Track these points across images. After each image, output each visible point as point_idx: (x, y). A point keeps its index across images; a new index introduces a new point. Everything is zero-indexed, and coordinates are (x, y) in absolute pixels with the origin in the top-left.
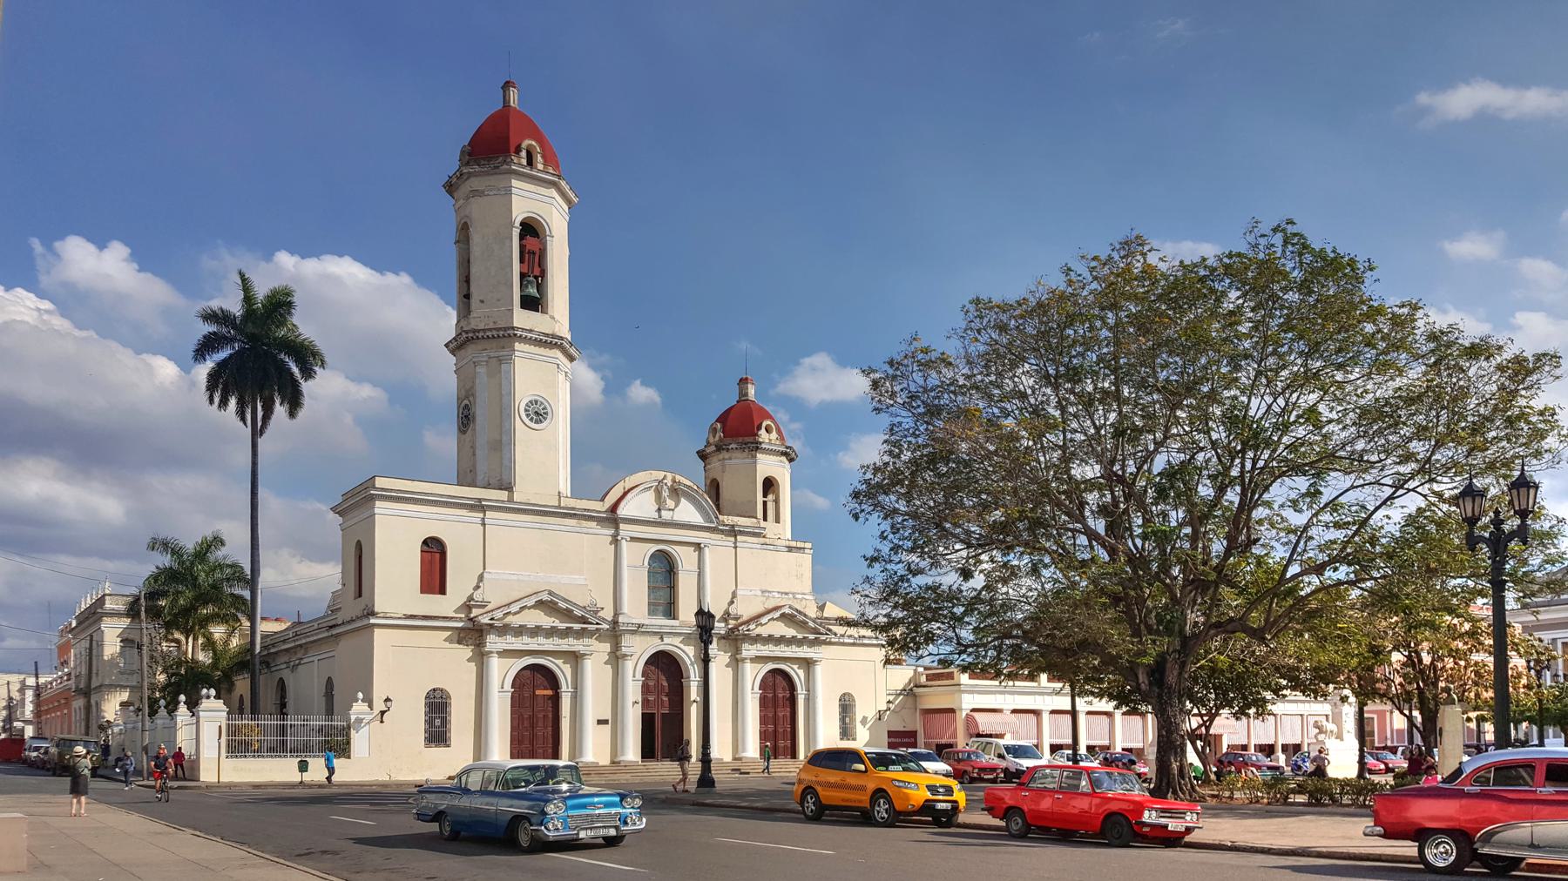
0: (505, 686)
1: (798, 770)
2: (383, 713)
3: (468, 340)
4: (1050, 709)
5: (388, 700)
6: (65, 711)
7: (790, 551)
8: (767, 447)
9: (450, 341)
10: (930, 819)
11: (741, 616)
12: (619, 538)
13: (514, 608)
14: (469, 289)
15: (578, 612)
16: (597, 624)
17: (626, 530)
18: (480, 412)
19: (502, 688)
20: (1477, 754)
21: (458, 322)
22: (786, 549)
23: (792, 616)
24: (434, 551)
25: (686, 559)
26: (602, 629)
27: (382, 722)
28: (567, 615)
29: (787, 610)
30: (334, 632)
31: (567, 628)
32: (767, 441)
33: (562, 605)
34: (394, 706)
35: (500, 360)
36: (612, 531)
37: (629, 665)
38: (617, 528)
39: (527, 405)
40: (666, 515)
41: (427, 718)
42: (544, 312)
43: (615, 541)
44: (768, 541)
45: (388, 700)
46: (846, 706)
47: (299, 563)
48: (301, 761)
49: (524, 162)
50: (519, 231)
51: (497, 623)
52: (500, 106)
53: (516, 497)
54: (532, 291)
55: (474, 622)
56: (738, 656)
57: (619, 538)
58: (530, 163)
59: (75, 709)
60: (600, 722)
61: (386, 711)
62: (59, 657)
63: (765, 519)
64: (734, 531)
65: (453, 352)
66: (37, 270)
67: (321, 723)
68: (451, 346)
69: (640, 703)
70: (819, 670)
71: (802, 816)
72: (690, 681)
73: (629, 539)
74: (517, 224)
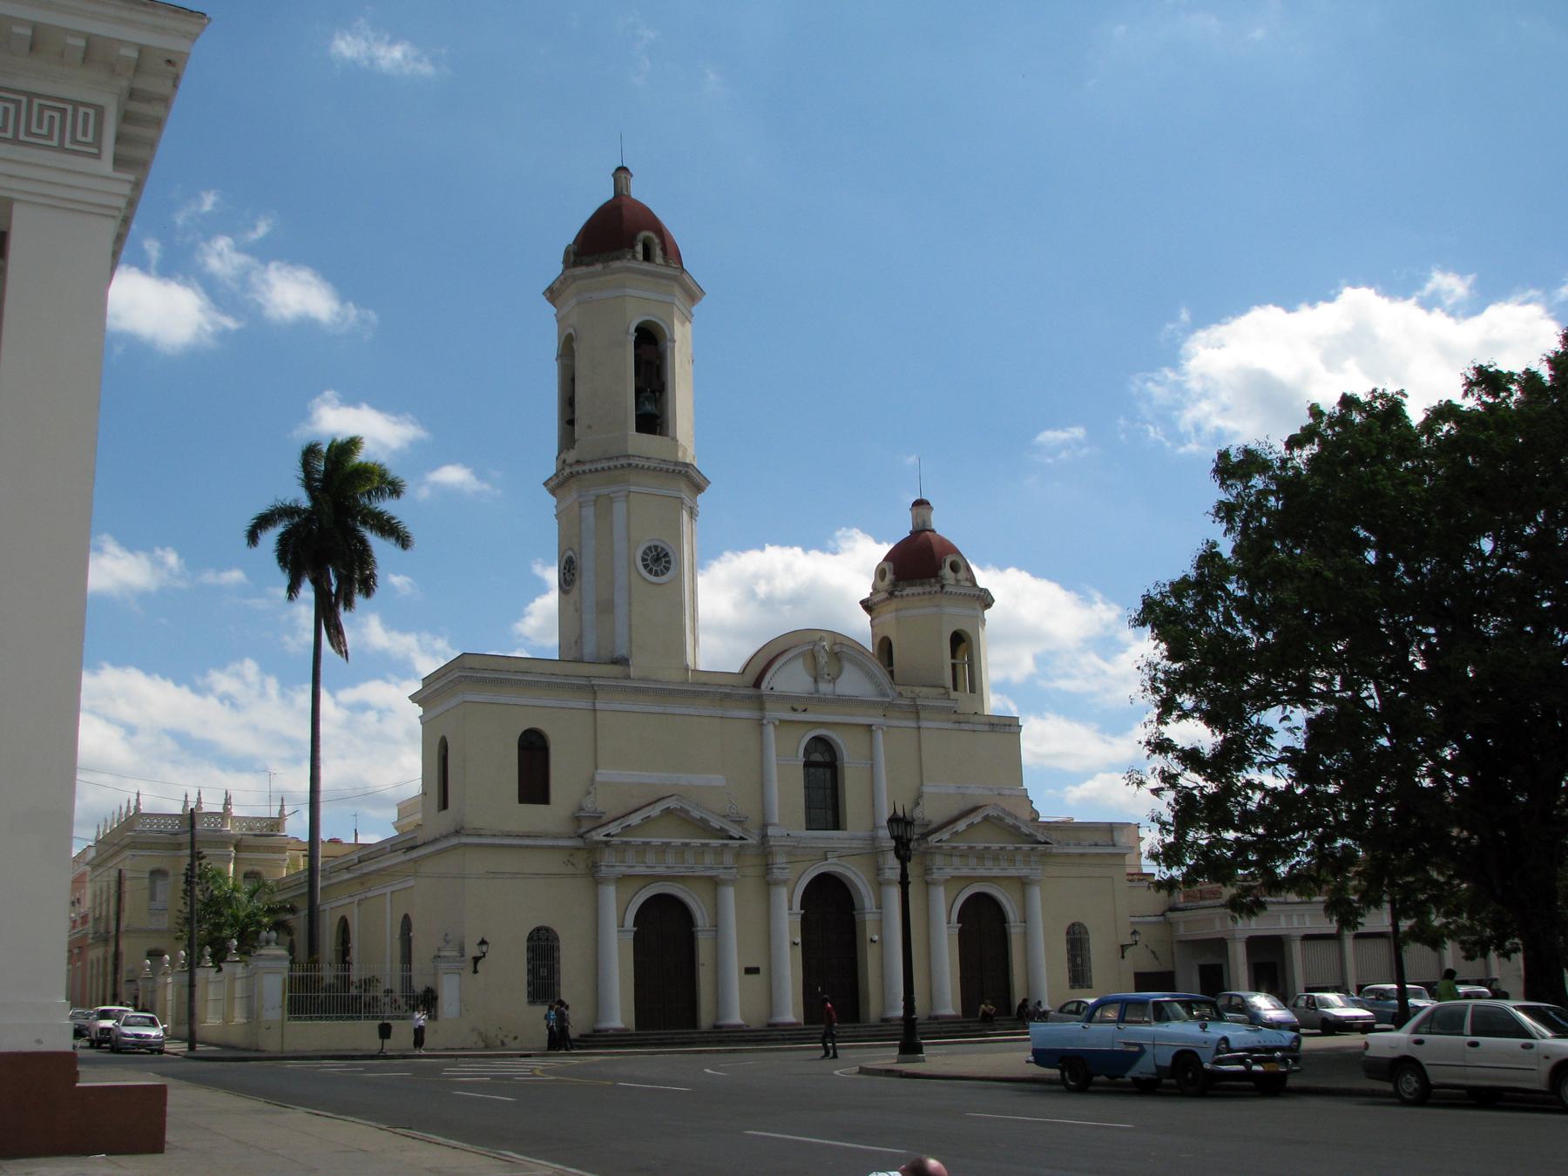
0: (626, 924)
1: (820, 1036)
2: (476, 960)
3: (572, 475)
4: (1303, 932)
5: (483, 942)
6: (79, 964)
7: (992, 731)
8: (954, 591)
9: (551, 478)
10: (1252, 1084)
11: (930, 822)
12: (765, 722)
13: (635, 819)
14: (573, 412)
15: (716, 823)
16: (741, 838)
17: (775, 713)
18: (587, 564)
19: (623, 926)
20: (433, 1016)
21: (559, 454)
22: (987, 728)
23: (1000, 819)
24: (534, 749)
25: (850, 751)
26: (748, 845)
27: (475, 972)
28: (703, 827)
29: (992, 812)
30: (414, 854)
31: (703, 845)
32: (953, 582)
33: (696, 814)
34: (492, 952)
35: (611, 499)
36: (756, 714)
37: (782, 893)
38: (762, 708)
39: (645, 553)
40: (825, 687)
41: (530, 967)
42: (667, 435)
43: (760, 724)
44: (961, 718)
45: (483, 942)
46: (1077, 941)
47: (604, 813)
48: (381, 1025)
49: (640, 256)
50: (634, 338)
51: (615, 840)
52: (610, 195)
53: (633, 672)
54: (649, 408)
55: (585, 839)
56: (928, 878)
57: (765, 722)
58: (647, 256)
59: (92, 963)
60: (750, 971)
61: (480, 958)
62: (73, 893)
63: (955, 689)
64: (916, 706)
65: (553, 492)
66: (1445, 949)
67: (301, 973)
68: (552, 484)
69: (800, 945)
70: (1036, 893)
71: (1063, 1088)
72: (864, 913)
73: (777, 723)
74: (632, 329)
